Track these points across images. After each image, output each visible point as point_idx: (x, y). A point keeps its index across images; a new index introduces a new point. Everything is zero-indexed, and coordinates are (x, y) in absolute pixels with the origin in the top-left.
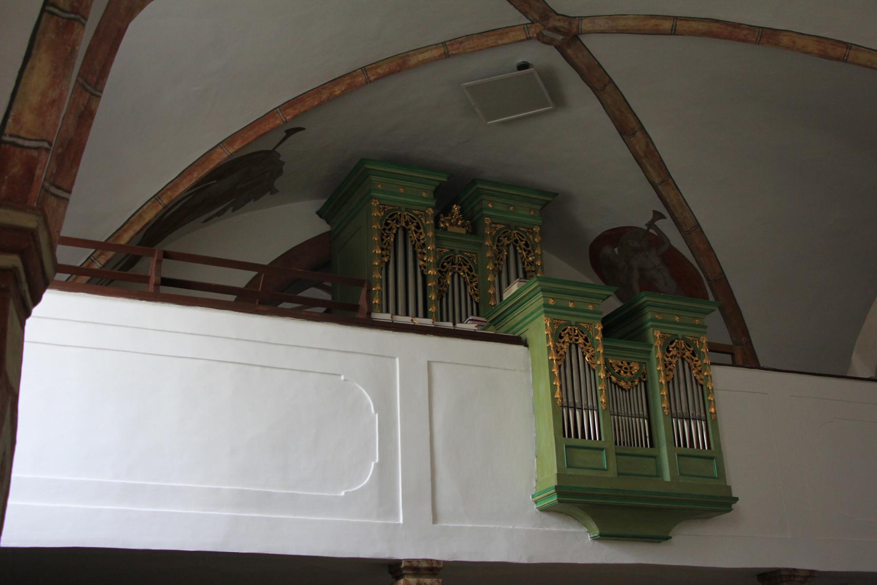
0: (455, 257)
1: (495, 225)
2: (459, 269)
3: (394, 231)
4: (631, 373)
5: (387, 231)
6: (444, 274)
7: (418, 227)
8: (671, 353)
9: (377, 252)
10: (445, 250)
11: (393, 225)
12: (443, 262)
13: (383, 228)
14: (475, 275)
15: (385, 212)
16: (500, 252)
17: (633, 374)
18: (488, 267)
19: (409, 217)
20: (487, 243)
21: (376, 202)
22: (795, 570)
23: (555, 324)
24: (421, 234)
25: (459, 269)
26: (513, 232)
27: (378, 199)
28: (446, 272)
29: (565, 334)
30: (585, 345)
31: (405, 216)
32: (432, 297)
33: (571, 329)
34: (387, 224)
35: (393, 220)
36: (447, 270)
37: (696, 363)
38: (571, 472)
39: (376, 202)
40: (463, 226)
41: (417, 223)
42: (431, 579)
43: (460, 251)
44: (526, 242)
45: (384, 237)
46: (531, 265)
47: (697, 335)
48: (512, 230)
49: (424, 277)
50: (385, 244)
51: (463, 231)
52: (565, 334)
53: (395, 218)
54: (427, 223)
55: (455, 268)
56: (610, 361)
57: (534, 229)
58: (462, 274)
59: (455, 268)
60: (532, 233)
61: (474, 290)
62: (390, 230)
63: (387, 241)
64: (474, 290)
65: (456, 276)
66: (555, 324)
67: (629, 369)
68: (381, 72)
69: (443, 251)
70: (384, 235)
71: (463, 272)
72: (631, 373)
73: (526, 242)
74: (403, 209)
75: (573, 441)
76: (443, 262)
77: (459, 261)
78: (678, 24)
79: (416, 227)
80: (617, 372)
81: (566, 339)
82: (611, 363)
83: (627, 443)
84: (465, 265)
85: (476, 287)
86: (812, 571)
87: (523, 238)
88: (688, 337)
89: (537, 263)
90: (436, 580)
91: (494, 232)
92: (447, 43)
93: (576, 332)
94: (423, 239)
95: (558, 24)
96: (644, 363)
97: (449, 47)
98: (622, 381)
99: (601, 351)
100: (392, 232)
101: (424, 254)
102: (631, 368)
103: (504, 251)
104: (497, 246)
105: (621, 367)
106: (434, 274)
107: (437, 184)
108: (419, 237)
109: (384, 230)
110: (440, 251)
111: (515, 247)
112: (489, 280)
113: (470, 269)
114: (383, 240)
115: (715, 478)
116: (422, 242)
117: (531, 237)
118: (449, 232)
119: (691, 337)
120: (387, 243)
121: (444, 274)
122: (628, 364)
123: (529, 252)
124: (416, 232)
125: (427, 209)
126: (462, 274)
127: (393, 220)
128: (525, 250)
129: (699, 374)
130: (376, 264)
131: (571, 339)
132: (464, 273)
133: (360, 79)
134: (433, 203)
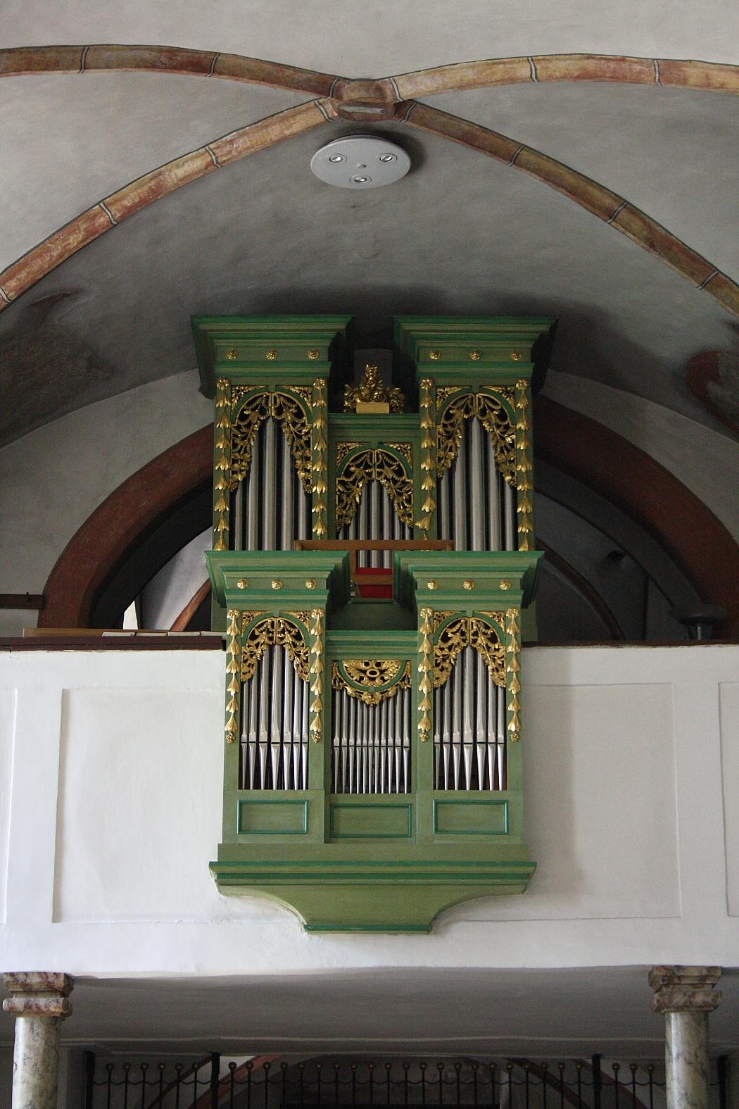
0: (371, 454)
1: (442, 390)
2: (380, 474)
3: (256, 427)
4: (382, 678)
5: (244, 430)
6: (350, 486)
7: (299, 414)
8: (450, 643)
9: (222, 468)
10: (353, 446)
11: (254, 416)
12: (349, 466)
13: (236, 425)
14: (407, 480)
15: (240, 398)
16: (450, 436)
17: (385, 681)
18: (423, 466)
19: (282, 398)
20: (424, 425)
21: (224, 384)
22: (679, 967)
23: (244, 618)
24: (303, 425)
25: (380, 474)
26: (477, 396)
27: (226, 378)
28: (353, 483)
29: (262, 632)
30: (295, 646)
31: (275, 398)
32: (317, 531)
33: (273, 623)
34: (243, 417)
35: (253, 410)
36: (355, 479)
37: (496, 653)
38: (242, 839)
39: (224, 384)
40: (384, 398)
41: (298, 408)
42: (46, 999)
43: (381, 443)
44: (502, 410)
45: (238, 441)
46: (508, 451)
47: (500, 607)
48: (475, 394)
49: (310, 497)
50: (239, 452)
51: (384, 408)
52: (262, 632)
53: (257, 405)
54: (314, 405)
55: (371, 473)
56: (345, 665)
57: (517, 385)
58: (383, 481)
59: (371, 473)
60: (513, 393)
61: (405, 507)
62: (248, 426)
63: (242, 447)
64: (405, 507)
65: (374, 485)
66: (244, 618)
67: (378, 673)
68: (129, 205)
69: (348, 447)
70: (238, 437)
71: (386, 478)
72: (382, 678)
73: (502, 410)
74: (273, 387)
75: (252, 794)
76: (349, 466)
77: (378, 460)
78: (538, 67)
79: (295, 414)
80: (356, 680)
81: (263, 638)
82: (346, 667)
83: (367, 786)
84: (390, 466)
85: (409, 501)
86: (711, 969)
87: (496, 404)
88: (486, 613)
89: (518, 447)
90: (55, 999)
91: (439, 404)
92: (212, 146)
93: (282, 626)
94: (307, 434)
95: (354, 95)
96: (407, 661)
97: (217, 151)
98: (365, 693)
99: (318, 653)
100: (253, 430)
101: (308, 459)
102: (382, 672)
103: (457, 433)
104: (445, 426)
105: (364, 672)
106: (322, 491)
107: (333, 334)
108: (300, 431)
109: (239, 427)
110: (344, 449)
111: (480, 422)
112: (423, 487)
113: (399, 472)
114: (235, 445)
115: (502, 833)
116: (305, 439)
117: (510, 401)
118: (358, 414)
119: (489, 611)
120: (243, 449)
121: (350, 486)
122: (378, 665)
123: (507, 427)
124: (294, 424)
125: (314, 381)
126: (383, 481)
127: (253, 410)
128: (498, 427)
129: (498, 671)
130: (220, 488)
131: (271, 639)
132: (388, 480)
133: (102, 219)
134: (326, 369)
